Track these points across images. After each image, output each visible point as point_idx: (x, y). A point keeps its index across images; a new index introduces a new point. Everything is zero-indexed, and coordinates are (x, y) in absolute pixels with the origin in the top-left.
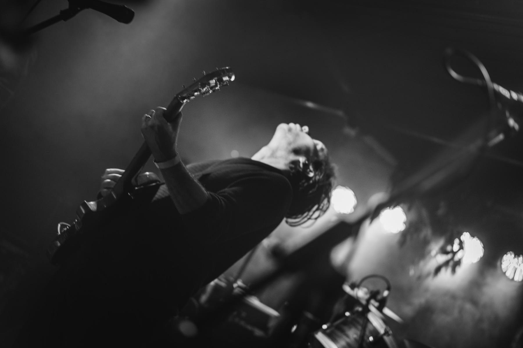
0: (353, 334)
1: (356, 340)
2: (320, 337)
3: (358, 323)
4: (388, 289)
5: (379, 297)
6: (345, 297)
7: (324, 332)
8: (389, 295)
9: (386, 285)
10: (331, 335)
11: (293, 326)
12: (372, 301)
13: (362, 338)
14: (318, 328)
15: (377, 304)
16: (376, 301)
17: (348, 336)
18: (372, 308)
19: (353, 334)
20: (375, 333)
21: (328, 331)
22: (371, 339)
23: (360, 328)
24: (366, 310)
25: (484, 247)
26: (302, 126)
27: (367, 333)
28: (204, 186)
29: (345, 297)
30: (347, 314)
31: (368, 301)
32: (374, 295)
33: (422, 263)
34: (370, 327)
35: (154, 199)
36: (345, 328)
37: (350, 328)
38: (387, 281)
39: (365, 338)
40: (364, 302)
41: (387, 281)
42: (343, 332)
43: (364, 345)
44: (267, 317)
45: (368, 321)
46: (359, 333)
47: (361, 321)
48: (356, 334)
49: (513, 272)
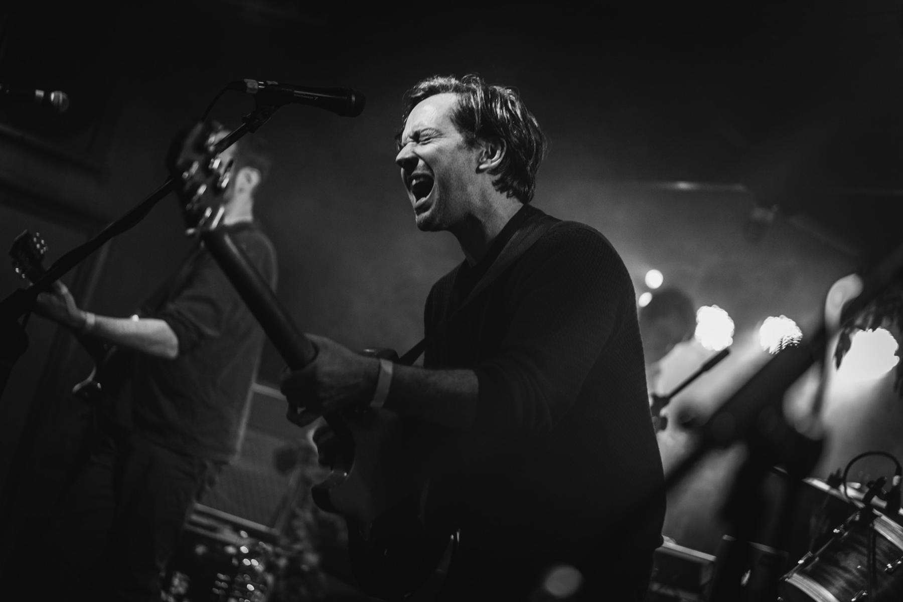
0: (854, 564)
2: (797, 580)
3: (883, 552)
4: (898, 473)
7: (802, 572)
8: (900, 481)
9: (894, 468)
10: (819, 576)
11: (743, 575)
14: (791, 566)
17: (846, 570)
19: (854, 564)
24: (868, 516)
28: (432, 213)
31: (867, 500)
32: (874, 487)
39: (878, 565)
42: (837, 564)
44: (696, 566)
49: (697, 367)
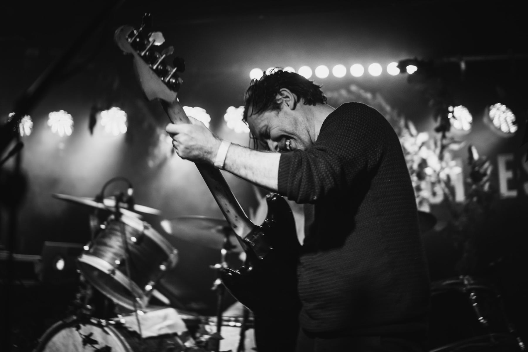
1: (120, 247)
2: (86, 259)
3: (117, 230)
5: (125, 199)
6: (96, 212)
7: (87, 253)
8: (134, 193)
12: (121, 204)
13: (126, 243)
15: (126, 205)
16: (124, 202)
17: (111, 247)
18: (123, 211)
20: (136, 233)
21: (92, 250)
22: (134, 239)
23: (119, 234)
24: (119, 215)
25: (207, 112)
26: (514, 123)
27: (128, 235)
29: (96, 212)
30: (103, 227)
32: (119, 199)
33: (156, 152)
34: (128, 230)
35: (302, 243)
36: (107, 241)
37: (110, 238)
38: (126, 180)
39: (128, 241)
40: (113, 209)
41: (126, 180)
42: (105, 245)
43: (130, 248)
45: (124, 224)
46: (120, 239)
47: (118, 228)
48: (119, 241)
